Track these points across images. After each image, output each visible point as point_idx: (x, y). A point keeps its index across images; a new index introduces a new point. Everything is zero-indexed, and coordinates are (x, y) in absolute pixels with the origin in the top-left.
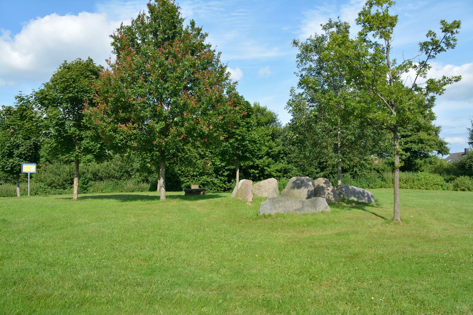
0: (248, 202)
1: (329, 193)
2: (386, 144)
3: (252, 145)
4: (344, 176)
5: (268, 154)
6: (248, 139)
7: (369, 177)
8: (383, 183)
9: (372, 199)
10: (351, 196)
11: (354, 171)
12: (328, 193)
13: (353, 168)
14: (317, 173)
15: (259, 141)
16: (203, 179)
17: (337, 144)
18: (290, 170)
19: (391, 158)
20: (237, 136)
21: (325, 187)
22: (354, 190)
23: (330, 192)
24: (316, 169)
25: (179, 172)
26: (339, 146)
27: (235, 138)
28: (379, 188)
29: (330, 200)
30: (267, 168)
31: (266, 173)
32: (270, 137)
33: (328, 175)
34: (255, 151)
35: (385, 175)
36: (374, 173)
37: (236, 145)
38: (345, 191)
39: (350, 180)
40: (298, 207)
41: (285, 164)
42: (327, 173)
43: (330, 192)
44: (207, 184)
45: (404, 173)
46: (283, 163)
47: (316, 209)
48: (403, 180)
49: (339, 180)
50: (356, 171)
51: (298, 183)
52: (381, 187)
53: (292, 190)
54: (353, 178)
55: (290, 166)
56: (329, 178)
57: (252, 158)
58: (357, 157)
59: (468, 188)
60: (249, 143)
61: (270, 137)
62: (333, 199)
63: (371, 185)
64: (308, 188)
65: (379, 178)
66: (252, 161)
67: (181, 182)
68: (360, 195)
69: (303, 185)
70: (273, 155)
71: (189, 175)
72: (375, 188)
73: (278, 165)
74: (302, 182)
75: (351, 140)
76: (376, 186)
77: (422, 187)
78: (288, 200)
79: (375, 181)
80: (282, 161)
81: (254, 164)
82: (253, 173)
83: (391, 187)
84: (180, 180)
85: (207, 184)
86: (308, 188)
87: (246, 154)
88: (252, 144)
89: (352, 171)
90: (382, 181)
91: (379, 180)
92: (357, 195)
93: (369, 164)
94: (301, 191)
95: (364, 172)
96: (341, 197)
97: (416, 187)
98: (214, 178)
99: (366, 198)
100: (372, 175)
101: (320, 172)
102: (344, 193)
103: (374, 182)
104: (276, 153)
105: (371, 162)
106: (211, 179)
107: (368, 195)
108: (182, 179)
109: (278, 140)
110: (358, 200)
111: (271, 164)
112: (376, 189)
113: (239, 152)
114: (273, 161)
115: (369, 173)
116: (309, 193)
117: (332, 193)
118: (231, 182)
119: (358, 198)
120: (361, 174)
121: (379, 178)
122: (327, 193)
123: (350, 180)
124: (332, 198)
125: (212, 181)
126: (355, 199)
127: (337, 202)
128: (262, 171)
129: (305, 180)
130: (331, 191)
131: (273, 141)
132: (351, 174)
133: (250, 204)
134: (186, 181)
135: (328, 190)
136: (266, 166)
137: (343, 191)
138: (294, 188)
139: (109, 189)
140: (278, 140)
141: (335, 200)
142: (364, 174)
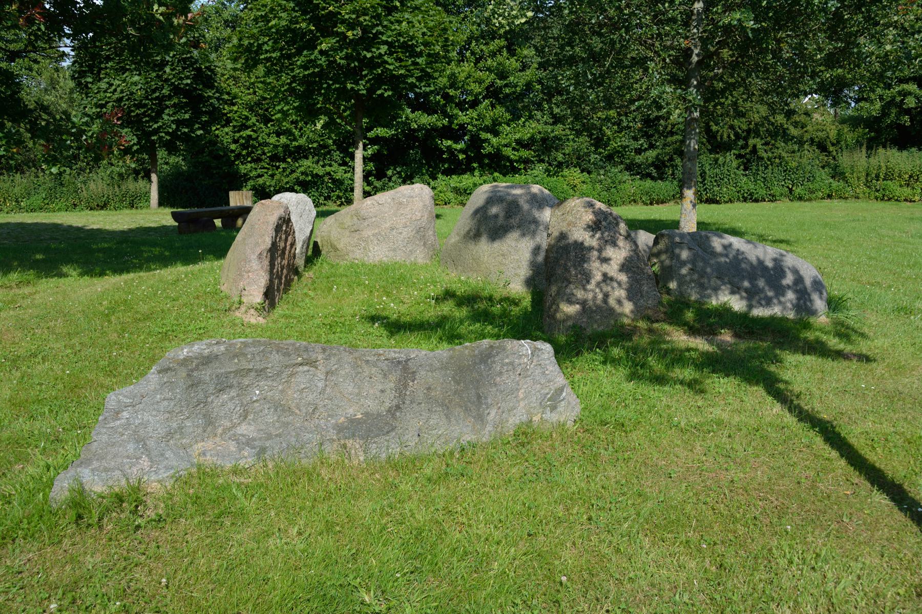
0: (243, 309)
1: (606, 278)
2: (888, 47)
3: (401, 60)
4: (716, 160)
5: (493, 93)
6: (384, 38)
7: (794, 164)
8: (835, 184)
9: (815, 297)
10: (716, 289)
11: (750, 148)
12: (605, 275)
13: (746, 139)
14: (639, 151)
15: (426, 44)
16: (302, 169)
17: (687, 53)
19: (867, 105)
20: (341, 29)
21: (591, 248)
22: (739, 258)
23: (612, 269)
24: (635, 139)
25: (233, 147)
26: (695, 59)
27: (337, 34)
28: (823, 198)
29: (611, 311)
30: (489, 136)
31: (487, 149)
32: (503, 42)
33: (671, 159)
34: (410, 80)
35: (845, 160)
36: (809, 154)
37: (339, 58)
38: (693, 261)
39: (735, 173)
40: (372, 405)
41: (546, 123)
43: (612, 269)
44: (315, 183)
45: (905, 153)
46: (538, 121)
47: (481, 418)
48: (900, 176)
49: (689, 188)
50: (755, 146)
51: (496, 216)
52: (830, 196)
53: (471, 246)
54: (746, 169)
55: (559, 130)
56: (672, 166)
57: (445, 105)
58: (762, 102)
60: (391, 54)
61: (503, 42)
62: (628, 307)
63: (798, 190)
64: (534, 234)
65: (823, 167)
66: (445, 114)
67: (241, 176)
68: (761, 283)
69: (514, 221)
70: (507, 95)
71: (263, 157)
72: (810, 200)
73: (524, 126)
74: (512, 208)
75: (743, 29)
76: (812, 192)
78: (312, 363)
79: (812, 179)
80: (539, 114)
81: (451, 122)
82: (449, 148)
83: (861, 195)
84: (237, 172)
85: (315, 183)
87: (379, 92)
88: (400, 55)
89: (742, 148)
90: (833, 177)
91: (823, 175)
92: (746, 284)
93: (796, 124)
95: (780, 151)
96: (668, 292)
98: (335, 165)
99: (790, 295)
100: (804, 161)
101: (646, 150)
102: (684, 271)
103: (809, 180)
104: (518, 89)
105: (803, 118)
106: (328, 169)
107: (799, 280)
108: (243, 169)
109: (525, 52)
110: (750, 307)
111: (500, 124)
112: (814, 203)
113: (357, 84)
114: (508, 116)
115: (794, 152)
116: (540, 258)
117: (623, 278)
118: (385, 175)
119: (752, 295)
120: (770, 155)
121: (823, 167)
122: (598, 277)
123: (735, 173)
124: (619, 302)
125: (329, 174)
126: (737, 304)
127: (642, 324)
128: (476, 143)
130: (624, 268)
131: (512, 53)
132: (738, 156)
133: (254, 319)
134: (254, 173)
135: (606, 260)
136: (487, 129)
137: (684, 264)
139: (37, 200)
140: (525, 52)
141: (639, 312)
142: (780, 157)
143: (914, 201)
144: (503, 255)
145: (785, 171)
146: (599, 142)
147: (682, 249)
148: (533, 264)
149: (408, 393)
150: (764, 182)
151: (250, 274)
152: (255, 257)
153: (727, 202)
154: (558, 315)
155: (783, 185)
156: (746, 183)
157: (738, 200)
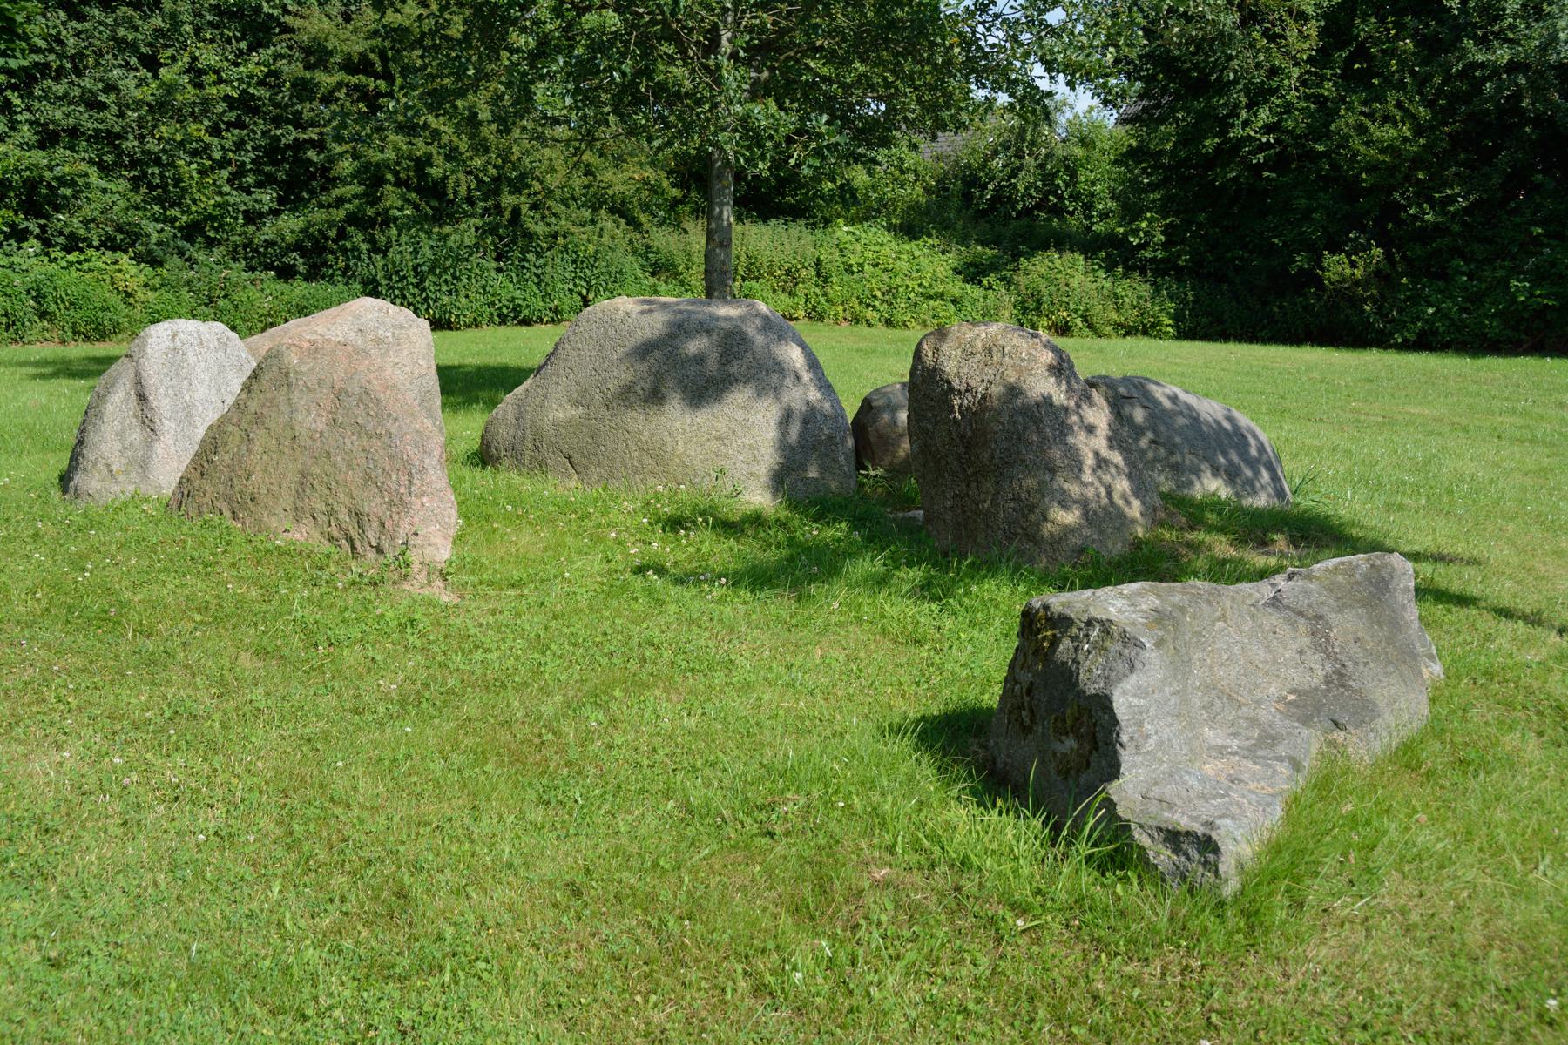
14: (252, 217)
18: (68, 192)
42: (331, 224)
51: (700, 359)
53: (636, 419)
59: (1085, 319)
64: (776, 391)
69: (735, 368)
77: (869, 313)
86: (776, 391)
94: (721, 425)
97: (840, 308)
129: (750, 330)
138: (655, 397)
143: (797, 319)
144: (718, 438)
145: (574, 262)
146: (167, 195)
147: (1133, 406)
148: (783, 446)
149: (1337, 650)
150: (538, 284)
151: (425, 499)
152: (434, 462)
153: (468, 326)
154: (1047, 529)
155: (571, 291)
156: (505, 287)
157: (491, 321)
